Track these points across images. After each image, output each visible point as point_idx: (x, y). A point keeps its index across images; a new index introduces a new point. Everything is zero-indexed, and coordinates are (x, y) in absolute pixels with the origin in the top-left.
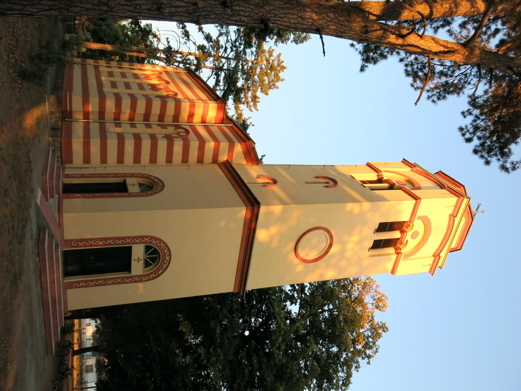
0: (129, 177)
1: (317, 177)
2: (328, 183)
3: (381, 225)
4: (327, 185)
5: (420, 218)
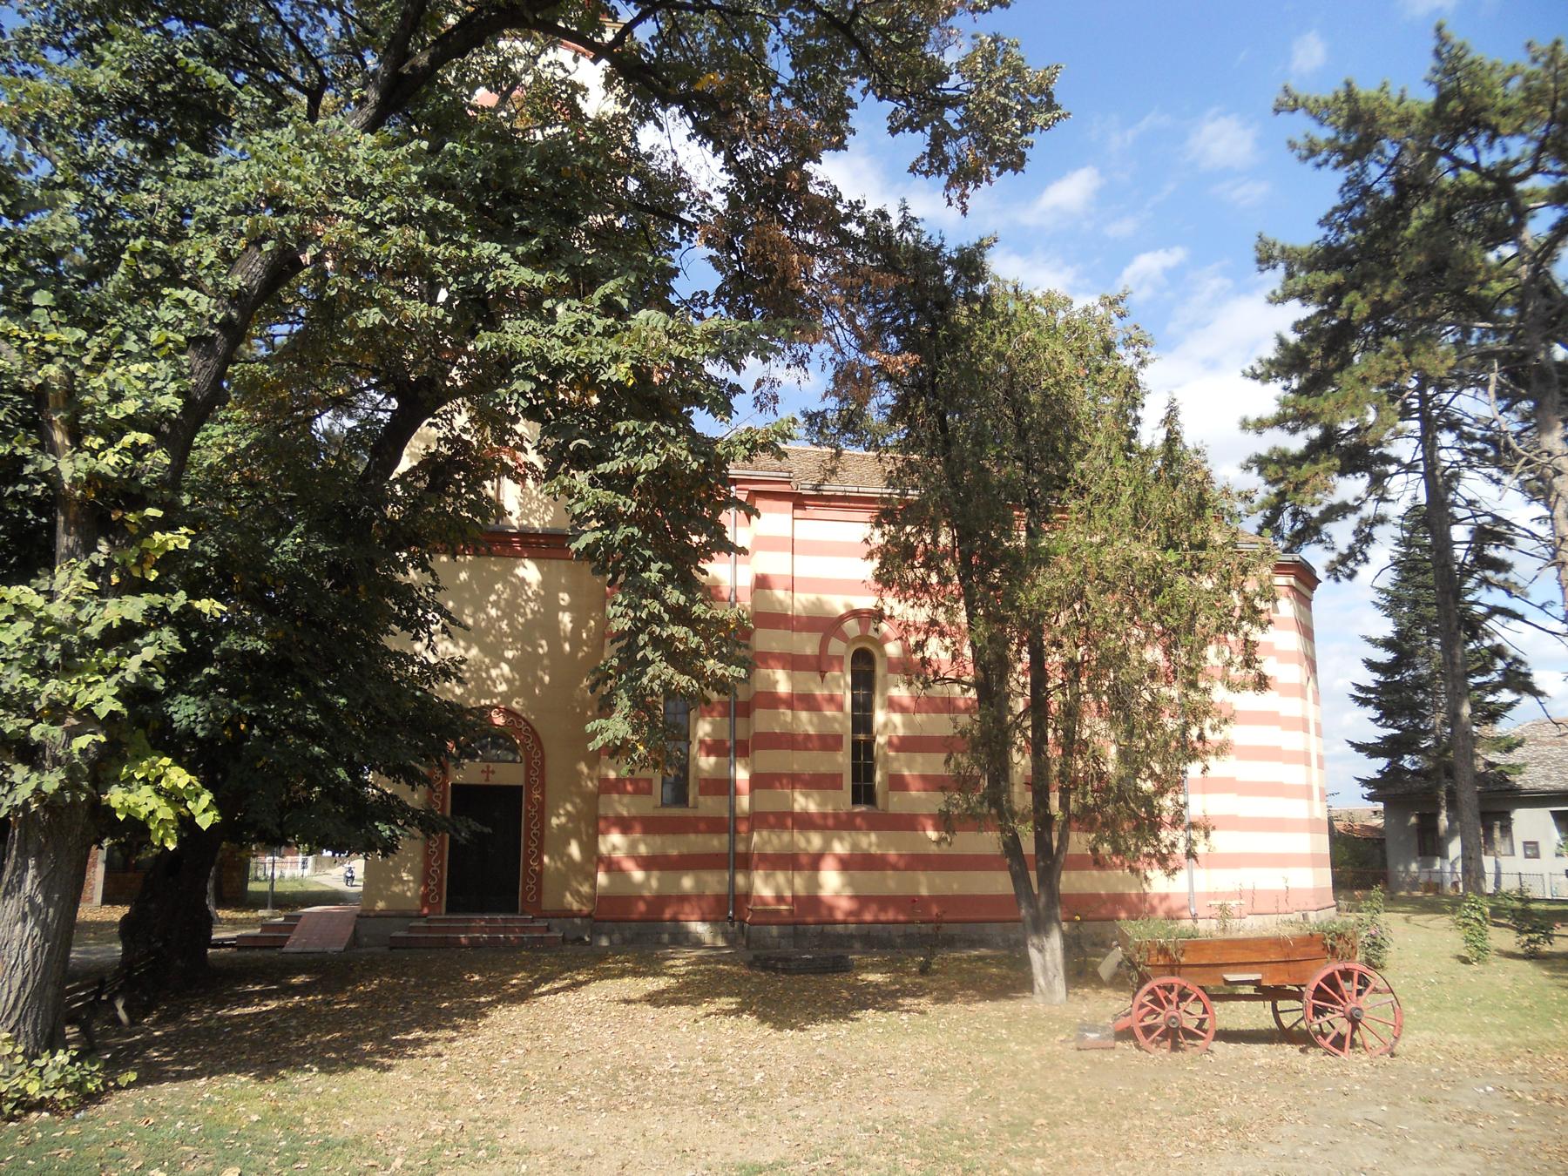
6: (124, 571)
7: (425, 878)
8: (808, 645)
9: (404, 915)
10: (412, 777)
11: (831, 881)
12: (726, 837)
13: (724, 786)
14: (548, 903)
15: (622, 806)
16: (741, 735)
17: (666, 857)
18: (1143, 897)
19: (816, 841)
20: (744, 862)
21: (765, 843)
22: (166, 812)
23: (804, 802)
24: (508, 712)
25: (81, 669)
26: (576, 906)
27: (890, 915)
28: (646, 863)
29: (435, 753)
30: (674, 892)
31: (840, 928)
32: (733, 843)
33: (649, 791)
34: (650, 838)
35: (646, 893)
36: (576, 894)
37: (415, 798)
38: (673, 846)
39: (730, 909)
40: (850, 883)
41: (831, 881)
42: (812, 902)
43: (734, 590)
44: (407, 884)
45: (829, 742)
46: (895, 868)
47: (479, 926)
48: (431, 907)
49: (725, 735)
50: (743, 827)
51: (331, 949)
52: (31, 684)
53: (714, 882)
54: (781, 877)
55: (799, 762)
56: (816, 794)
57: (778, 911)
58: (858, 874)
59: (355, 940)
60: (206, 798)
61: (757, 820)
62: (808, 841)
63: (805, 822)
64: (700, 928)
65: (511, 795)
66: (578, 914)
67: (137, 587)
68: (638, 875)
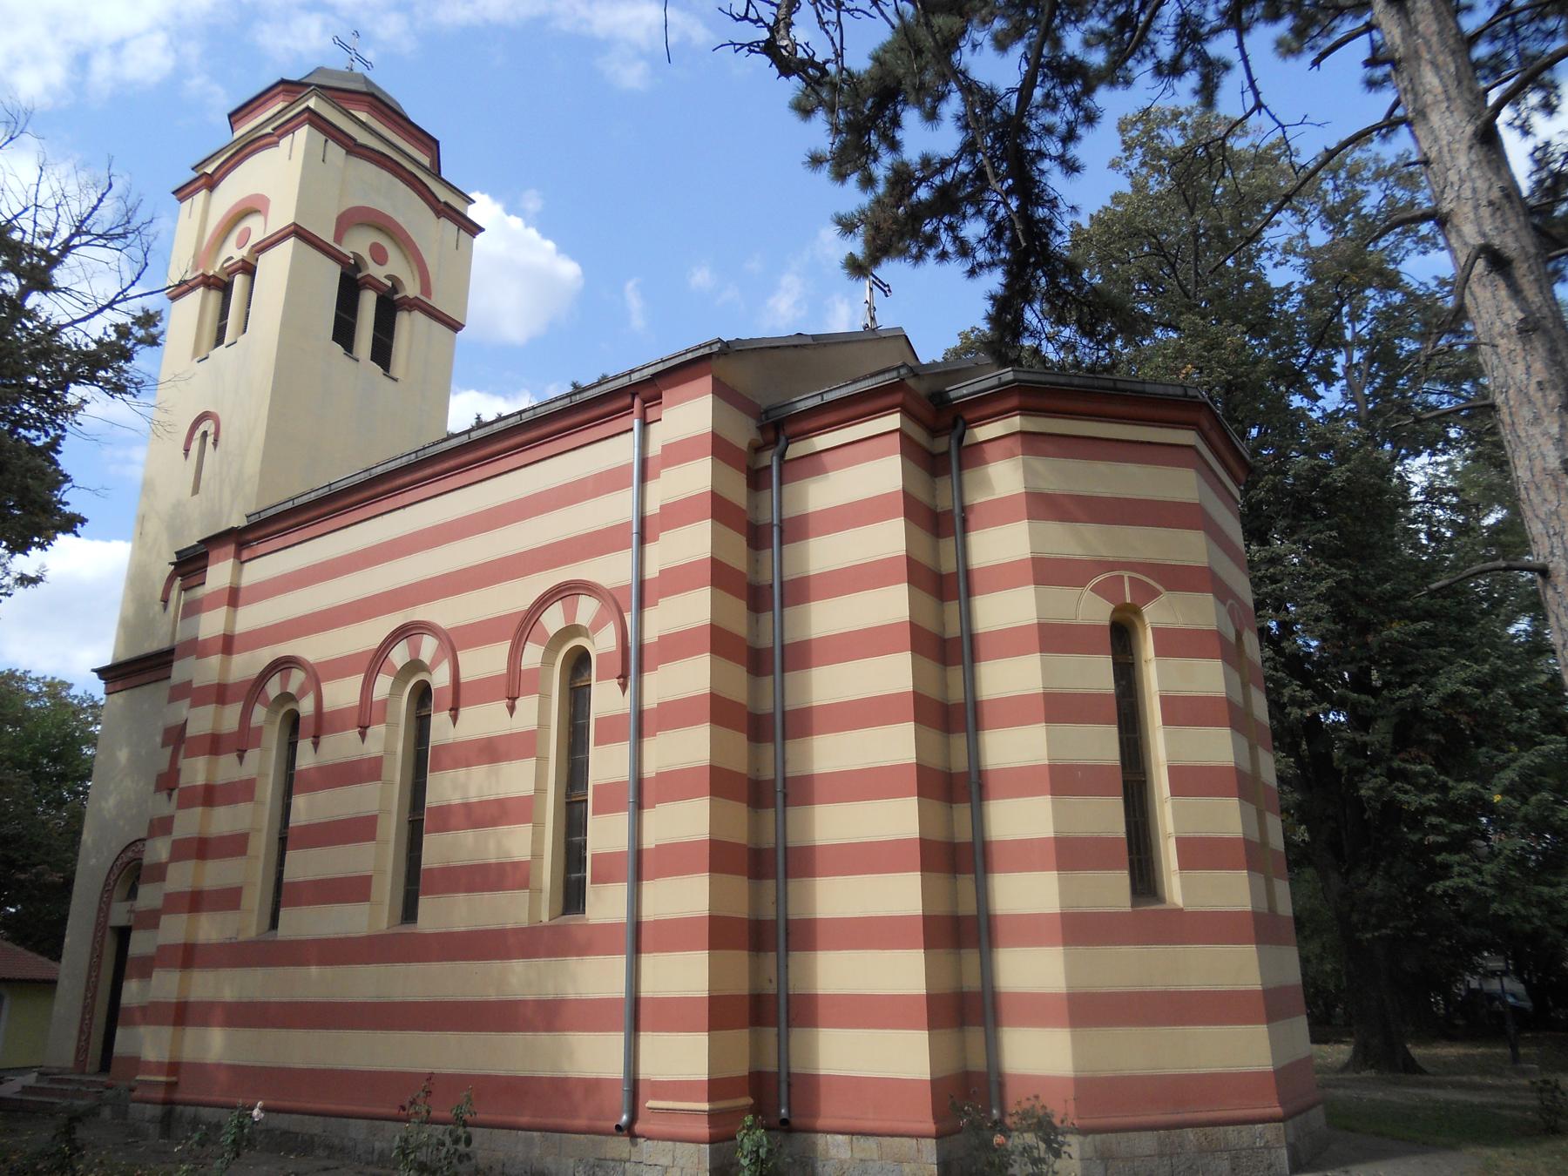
0: (107, 916)
1: (187, 450)
2: (205, 434)
3: (336, 338)
4: (210, 439)
5: (338, 237)
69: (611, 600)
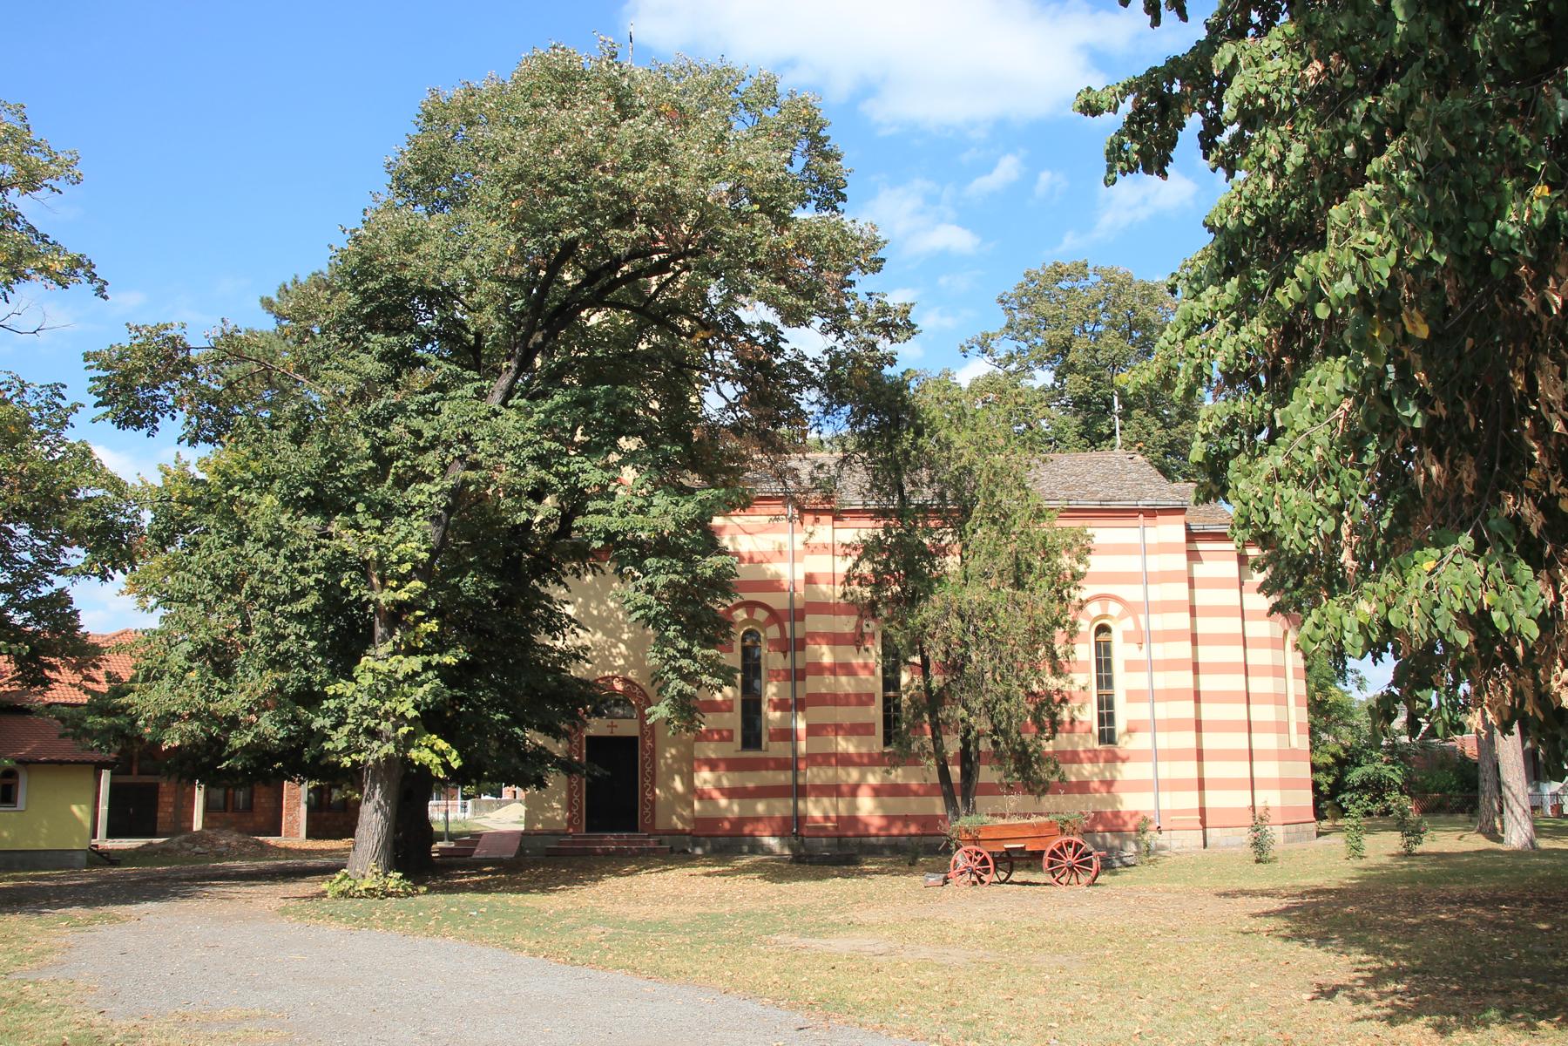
6: (408, 644)
7: (570, 806)
8: (846, 624)
9: (555, 833)
10: (557, 734)
11: (866, 805)
12: (790, 774)
13: (788, 735)
14: (660, 824)
15: (711, 750)
16: (800, 695)
17: (745, 788)
18: (1117, 814)
19: (854, 774)
20: (800, 792)
21: (814, 776)
22: (437, 760)
23: (845, 745)
24: (626, 681)
25: (395, 695)
26: (680, 826)
27: (913, 829)
28: (731, 793)
29: (572, 716)
30: (750, 814)
31: (873, 840)
32: (796, 777)
33: (730, 739)
34: (730, 775)
35: (729, 815)
36: (681, 817)
37: (559, 748)
38: (751, 781)
39: (794, 827)
40: (881, 806)
41: (866, 805)
42: (853, 820)
43: (793, 583)
44: (557, 812)
45: (864, 699)
46: (916, 794)
47: (611, 840)
48: (575, 827)
49: (788, 695)
50: (802, 765)
51: (505, 856)
52: (377, 703)
53: (782, 807)
54: (826, 801)
55: (844, 715)
56: (855, 739)
57: (825, 828)
58: (886, 799)
59: (521, 850)
60: (455, 753)
61: (812, 759)
62: (848, 775)
63: (845, 760)
64: (772, 842)
65: (630, 743)
66: (682, 833)
67: (412, 651)
68: (723, 802)
69: (1130, 608)
